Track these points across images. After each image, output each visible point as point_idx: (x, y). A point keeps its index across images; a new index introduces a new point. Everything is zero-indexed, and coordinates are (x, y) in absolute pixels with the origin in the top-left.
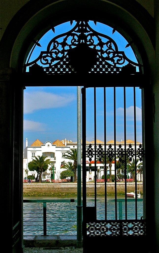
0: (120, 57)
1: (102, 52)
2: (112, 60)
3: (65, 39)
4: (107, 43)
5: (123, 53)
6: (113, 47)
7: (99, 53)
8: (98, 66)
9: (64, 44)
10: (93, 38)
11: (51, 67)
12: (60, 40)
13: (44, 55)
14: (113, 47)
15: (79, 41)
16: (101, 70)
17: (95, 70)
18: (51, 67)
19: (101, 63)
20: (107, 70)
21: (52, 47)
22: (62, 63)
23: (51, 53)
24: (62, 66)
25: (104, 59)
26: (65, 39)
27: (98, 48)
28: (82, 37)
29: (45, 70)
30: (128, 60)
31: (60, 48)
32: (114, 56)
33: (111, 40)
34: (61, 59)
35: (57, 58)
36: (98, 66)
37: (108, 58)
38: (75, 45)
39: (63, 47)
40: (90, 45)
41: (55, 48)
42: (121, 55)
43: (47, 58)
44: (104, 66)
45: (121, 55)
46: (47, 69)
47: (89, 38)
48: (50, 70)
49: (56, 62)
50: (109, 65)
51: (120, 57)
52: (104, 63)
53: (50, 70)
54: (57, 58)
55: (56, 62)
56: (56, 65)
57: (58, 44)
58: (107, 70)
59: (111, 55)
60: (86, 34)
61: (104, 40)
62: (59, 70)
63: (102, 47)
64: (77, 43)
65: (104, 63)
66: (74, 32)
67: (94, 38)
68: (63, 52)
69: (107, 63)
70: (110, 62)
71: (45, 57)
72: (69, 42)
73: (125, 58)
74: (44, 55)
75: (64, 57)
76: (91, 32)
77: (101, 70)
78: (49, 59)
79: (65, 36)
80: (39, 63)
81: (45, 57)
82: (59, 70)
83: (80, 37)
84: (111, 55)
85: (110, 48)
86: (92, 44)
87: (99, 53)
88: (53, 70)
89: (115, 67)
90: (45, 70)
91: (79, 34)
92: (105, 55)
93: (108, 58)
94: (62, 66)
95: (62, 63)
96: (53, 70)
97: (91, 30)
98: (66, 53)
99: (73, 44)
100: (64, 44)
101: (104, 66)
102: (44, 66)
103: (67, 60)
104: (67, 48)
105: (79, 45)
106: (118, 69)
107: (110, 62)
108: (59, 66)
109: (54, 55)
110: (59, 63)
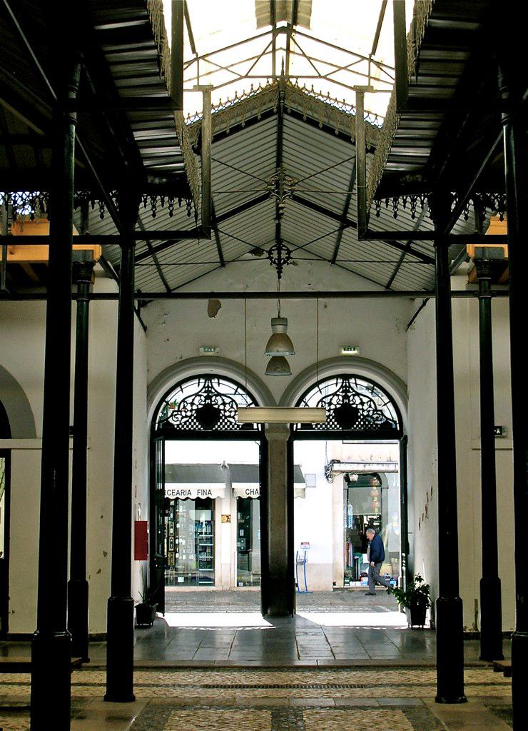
0: (379, 414)
1: (225, 411)
2: (233, 417)
3: (331, 399)
4: (229, 403)
5: (381, 411)
6: (373, 406)
7: (361, 411)
8: (221, 424)
9: (192, 404)
10: (217, 398)
11: (181, 424)
12: (190, 400)
13: (175, 413)
14: (373, 406)
15: (343, 401)
16: (192, 426)
17: (219, 426)
18: (181, 424)
19: (223, 421)
20: (228, 426)
21: (182, 406)
22: (190, 420)
23: (181, 411)
24: (190, 423)
25: (226, 417)
26: (331, 399)
27: (222, 407)
28: (208, 397)
29: (176, 426)
30: (386, 417)
31: (189, 407)
32: (373, 414)
33: (371, 400)
34: (190, 417)
35: (186, 416)
36: (221, 424)
37: (230, 416)
38: (340, 404)
39: (192, 406)
40: (353, 404)
41: (184, 407)
42: (380, 413)
43: (177, 416)
44: (226, 424)
45: (380, 413)
46: (178, 425)
47: (213, 398)
48: (180, 426)
49: (185, 420)
50: (231, 423)
51: (379, 414)
52: (226, 421)
53: (180, 426)
54: (186, 416)
55: (185, 420)
56: (185, 423)
57: (325, 403)
58: (228, 426)
59: (232, 414)
60: (349, 394)
61: (227, 400)
62: (188, 426)
63: (363, 406)
64: (341, 403)
65: (226, 421)
66: (200, 393)
67: (356, 398)
68: (191, 411)
69: (228, 421)
70: (231, 420)
71: (176, 415)
72: (334, 401)
73: (383, 415)
74: (175, 413)
75: (192, 415)
76: (354, 393)
77: (192, 426)
78: (180, 417)
79: (194, 397)
80: (170, 420)
81: (176, 415)
82: (188, 426)
83: (207, 398)
84: (371, 413)
85: (370, 406)
86: (216, 404)
87: (361, 411)
88: (183, 426)
89: (235, 424)
90: (176, 426)
91: (205, 394)
92: (227, 414)
93: (230, 416)
94: (190, 423)
95: (190, 420)
96: (183, 426)
97: (354, 391)
98: (332, 411)
99: (338, 404)
100: (192, 404)
101: (226, 424)
102: (174, 423)
103: (333, 417)
104: (333, 407)
105: (344, 405)
106: (377, 425)
107: (231, 420)
108: (188, 423)
109: (184, 414)
110: (188, 421)
